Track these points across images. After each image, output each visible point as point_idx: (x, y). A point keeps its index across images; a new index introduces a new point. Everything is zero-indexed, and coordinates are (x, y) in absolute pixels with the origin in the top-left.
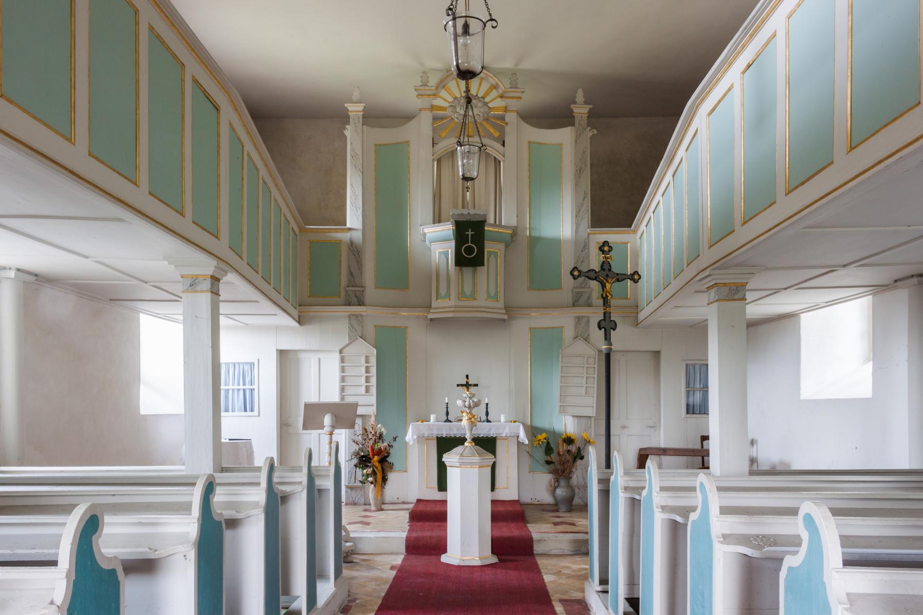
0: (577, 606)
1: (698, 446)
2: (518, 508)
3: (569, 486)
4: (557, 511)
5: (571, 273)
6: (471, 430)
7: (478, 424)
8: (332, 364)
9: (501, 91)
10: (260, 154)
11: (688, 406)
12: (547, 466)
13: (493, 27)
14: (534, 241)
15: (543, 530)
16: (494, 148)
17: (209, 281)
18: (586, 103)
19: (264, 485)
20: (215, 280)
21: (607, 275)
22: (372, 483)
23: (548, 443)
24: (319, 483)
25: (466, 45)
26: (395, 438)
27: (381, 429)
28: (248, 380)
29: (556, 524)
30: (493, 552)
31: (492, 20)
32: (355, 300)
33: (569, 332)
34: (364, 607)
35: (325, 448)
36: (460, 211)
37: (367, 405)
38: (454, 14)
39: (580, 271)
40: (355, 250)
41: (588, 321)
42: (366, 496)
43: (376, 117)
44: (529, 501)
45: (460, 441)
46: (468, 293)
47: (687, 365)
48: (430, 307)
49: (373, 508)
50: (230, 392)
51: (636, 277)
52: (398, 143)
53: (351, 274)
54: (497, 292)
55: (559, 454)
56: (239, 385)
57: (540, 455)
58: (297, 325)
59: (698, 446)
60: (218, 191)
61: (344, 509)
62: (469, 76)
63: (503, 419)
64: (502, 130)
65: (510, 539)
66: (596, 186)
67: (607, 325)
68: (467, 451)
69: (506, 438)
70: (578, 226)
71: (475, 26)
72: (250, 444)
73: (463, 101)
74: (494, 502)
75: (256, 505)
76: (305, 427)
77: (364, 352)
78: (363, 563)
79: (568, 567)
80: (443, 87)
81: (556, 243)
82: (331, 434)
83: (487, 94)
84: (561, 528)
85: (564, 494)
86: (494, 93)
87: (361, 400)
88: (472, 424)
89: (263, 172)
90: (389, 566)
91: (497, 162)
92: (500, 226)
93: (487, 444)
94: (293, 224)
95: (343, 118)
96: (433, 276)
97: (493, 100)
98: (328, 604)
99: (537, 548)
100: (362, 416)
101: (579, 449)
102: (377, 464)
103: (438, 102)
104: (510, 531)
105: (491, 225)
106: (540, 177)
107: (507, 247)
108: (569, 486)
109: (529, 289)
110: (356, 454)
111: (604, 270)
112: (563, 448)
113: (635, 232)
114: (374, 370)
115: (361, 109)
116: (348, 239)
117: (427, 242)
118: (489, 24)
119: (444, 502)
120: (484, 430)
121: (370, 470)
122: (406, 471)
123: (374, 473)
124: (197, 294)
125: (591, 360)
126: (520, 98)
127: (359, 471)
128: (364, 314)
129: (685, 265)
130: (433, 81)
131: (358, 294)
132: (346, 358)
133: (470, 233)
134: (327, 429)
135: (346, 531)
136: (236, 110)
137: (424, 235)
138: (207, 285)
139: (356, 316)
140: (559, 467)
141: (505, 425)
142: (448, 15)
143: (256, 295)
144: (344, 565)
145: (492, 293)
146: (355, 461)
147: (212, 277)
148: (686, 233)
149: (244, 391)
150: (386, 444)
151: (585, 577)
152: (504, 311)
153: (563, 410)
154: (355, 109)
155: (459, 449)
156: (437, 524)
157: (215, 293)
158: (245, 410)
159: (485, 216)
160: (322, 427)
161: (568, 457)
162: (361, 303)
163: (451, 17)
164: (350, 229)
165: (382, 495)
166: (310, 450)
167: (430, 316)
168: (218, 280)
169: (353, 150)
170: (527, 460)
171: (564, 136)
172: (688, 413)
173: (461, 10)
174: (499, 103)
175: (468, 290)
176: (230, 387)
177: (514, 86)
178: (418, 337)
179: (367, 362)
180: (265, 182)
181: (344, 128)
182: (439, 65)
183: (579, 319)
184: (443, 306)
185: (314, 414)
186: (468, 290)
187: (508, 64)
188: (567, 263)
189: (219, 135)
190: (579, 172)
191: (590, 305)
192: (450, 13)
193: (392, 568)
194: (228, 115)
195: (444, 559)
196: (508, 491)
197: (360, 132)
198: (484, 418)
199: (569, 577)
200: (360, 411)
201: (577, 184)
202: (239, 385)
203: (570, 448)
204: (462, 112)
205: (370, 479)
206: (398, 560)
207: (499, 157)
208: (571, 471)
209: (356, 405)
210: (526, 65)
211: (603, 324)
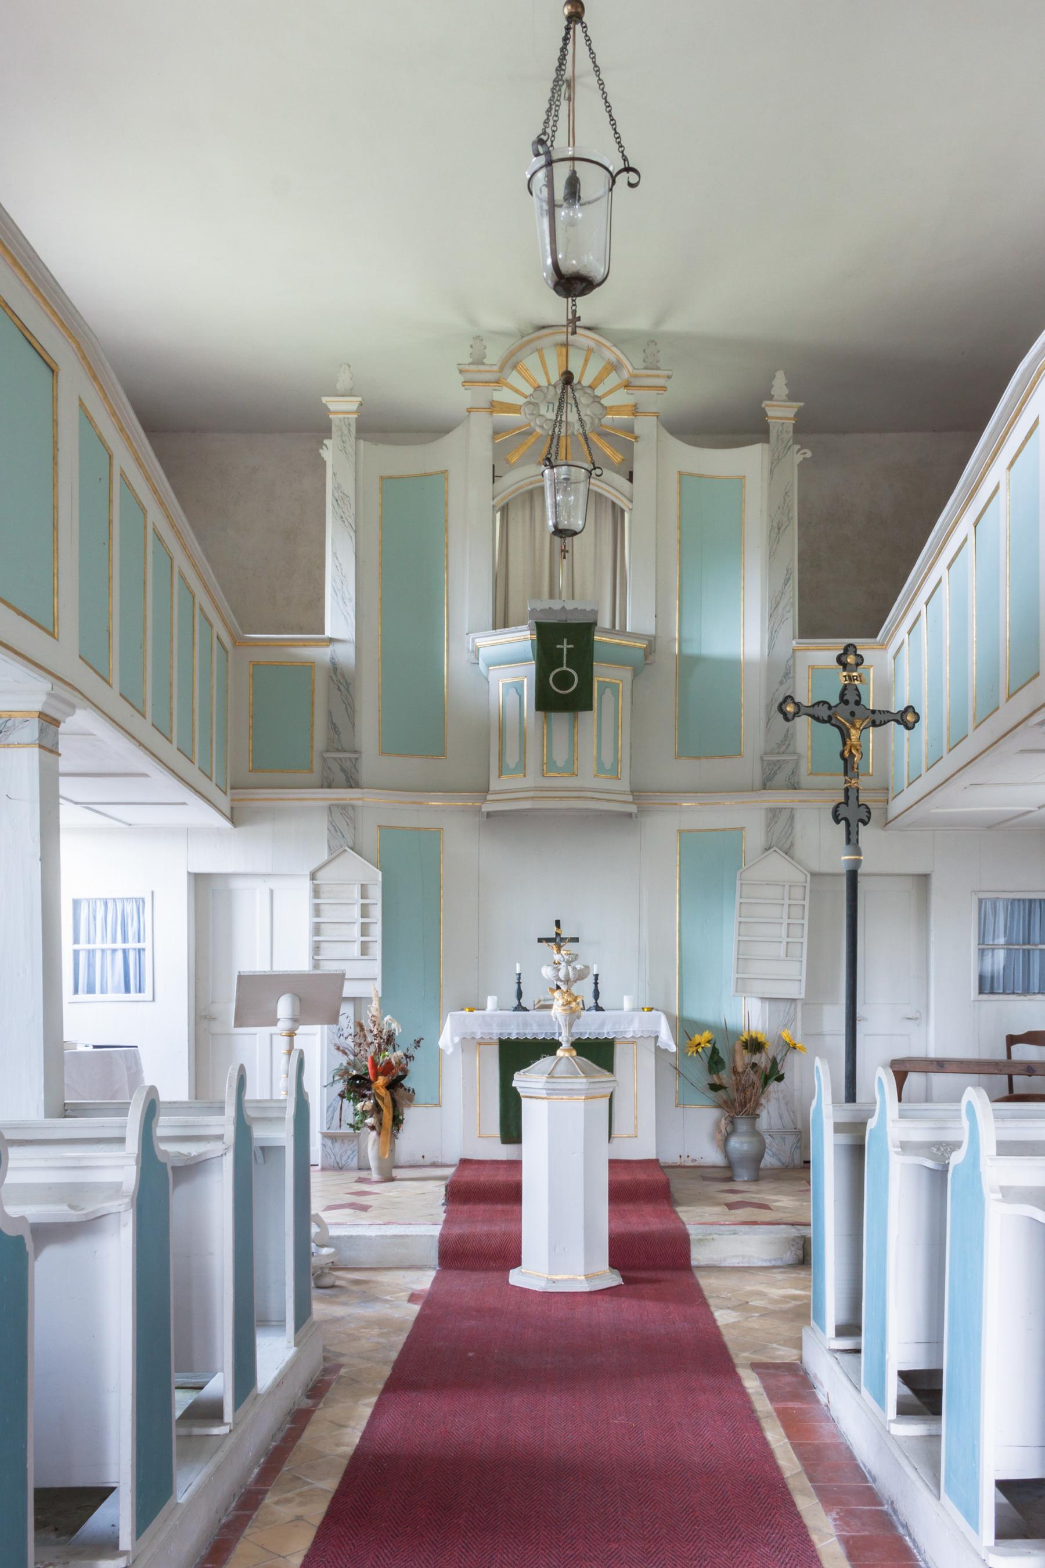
0: (790, 1379)
1: (1002, 1056)
2: (658, 1177)
3: (755, 1133)
4: (731, 1179)
5: (781, 709)
6: (570, 1026)
7: (584, 1013)
8: (295, 900)
9: (625, 375)
10: (148, 478)
11: (981, 978)
12: (712, 1094)
13: (631, 185)
14: (689, 665)
15: (708, 1218)
16: (611, 486)
17: (35, 724)
18: (792, 397)
19: (133, 1145)
20: (49, 722)
21: (853, 714)
22: (373, 1128)
23: (715, 1051)
24: (261, 1134)
25: (572, 223)
26: (419, 1042)
27: (391, 1023)
28: (131, 931)
29: (731, 1206)
30: (612, 1265)
31: (628, 169)
32: (341, 777)
33: (755, 837)
34: (355, 1385)
35: (281, 1061)
36: (545, 603)
37: (364, 978)
38: (548, 153)
39: (798, 705)
40: (341, 681)
41: (792, 818)
42: (361, 1155)
43: (379, 426)
44: (677, 1161)
45: (549, 1047)
46: (560, 763)
47: (980, 901)
48: (487, 791)
49: (375, 1176)
50: (98, 955)
51: (910, 718)
52: (425, 475)
53: (333, 727)
54: (616, 761)
55: (735, 1072)
56: (114, 941)
57: (699, 1073)
58: (226, 824)
59: (1002, 1056)
60: (55, 539)
61: (316, 1178)
62: (579, 286)
63: (627, 1004)
64: (627, 449)
65: (645, 1238)
66: (810, 563)
67: (852, 814)
68: (562, 1067)
69: (633, 1041)
70: (773, 635)
71: (592, 182)
72: (136, 1058)
73: (554, 394)
74: (613, 1164)
75: (116, 1189)
76: (240, 1022)
77: (358, 876)
78: (355, 1288)
79: (761, 1294)
80: (515, 367)
81: (732, 667)
82: (291, 1035)
83: (599, 380)
84: (741, 1214)
85: (745, 1147)
86: (613, 380)
87: (352, 970)
88: (573, 1016)
89: (155, 516)
90: (405, 1295)
91: (618, 513)
92: (623, 633)
93: (598, 1052)
94: (219, 628)
95: (320, 428)
96: (491, 733)
97: (611, 391)
98: (279, 1383)
99: (699, 1256)
100: (353, 999)
101: (774, 1062)
102: (383, 1092)
103: (504, 395)
104: (645, 1221)
105: (605, 632)
106: (701, 541)
107: (636, 674)
108: (755, 1133)
109: (678, 756)
110: (343, 1073)
111: (846, 702)
112: (743, 1059)
113: (884, 646)
114: (377, 912)
115: (354, 407)
116: (328, 658)
117: (482, 665)
118: (622, 179)
119: (516, 1165)
120: (591, 1026)
121: (369, 1104)
122: (439, 1105)
123: (377, 1109)
124: (10, 750)
125: (798, 892)
126: (663, 388)
127: (348, 1105)
128: (359, 803)
129: (1003, 695)
130: (494, 355)
131: (348, 765)
132: (324, 889)
133: (565, 646)
134: (283, 1025)
135: (321, 1224)
136: (95, 377)
137: (476, 651)
138: (30, 731)
139: (344, 808)
140: (735, 1095)
141: (632, 1017)
142: (537, 155)
143: (140, 761)
144: (315, 1293)
145: (608, 760)
146: (340, 1086)
147: (42, 715)
148: (1005, 634)
149: (125, 951)
150: (399, 1053)
151: (804, 1313)
152: (630, 798)
153: (742, 986)
154: (342, 408)
155: (545, 1063)
156: (499, 1207)
157: (49, 748)
158: (127, 990)
159: (595, 612)
160: (272, 1020)
161: (753, 1077)
162: (352, 783)
163: (542, 160)
164: (331, 640)
165: (392, 1151)
166: (242, 1068)
167: (487, 808)
168: (57, 723)
169: (337, 488)
170: (672, 1081)
171: (747, 462)
172: (981, 992)
173: (561, 146)
174: (621, 398)
175: (560, 757)
176: (98, 945)
177: (651, 365)
178: (463, 848)
179: (364, 915)
180: (159, 537)
181: (321, 444)
182: (506, 323)
183: (774, 814)
184: (509, 788)
185: (255, 997)
186: (560, 757)
187: (641, 322)
188: (754, 702)
189: (55, 422)
190: (776, 530)
191: (794, 786)
192: (541, 150)
193: (413, 1298)
194: (74, 383)
195: (516, 1278)
196: (641, 1146)
197: (351, 450)
198: (590, 1002)
199: (766, 1313)
200: (349, 990)
201: (772, 554)
202: (114, 941)
203: (756, 1058)
204: (552, 415)
205: (370, 1121)
206: (424, 1281)
207: (622, 503)
208: (758, 1104)
209: (340, 979)
210: (675, 325)
211: (843, 811)
